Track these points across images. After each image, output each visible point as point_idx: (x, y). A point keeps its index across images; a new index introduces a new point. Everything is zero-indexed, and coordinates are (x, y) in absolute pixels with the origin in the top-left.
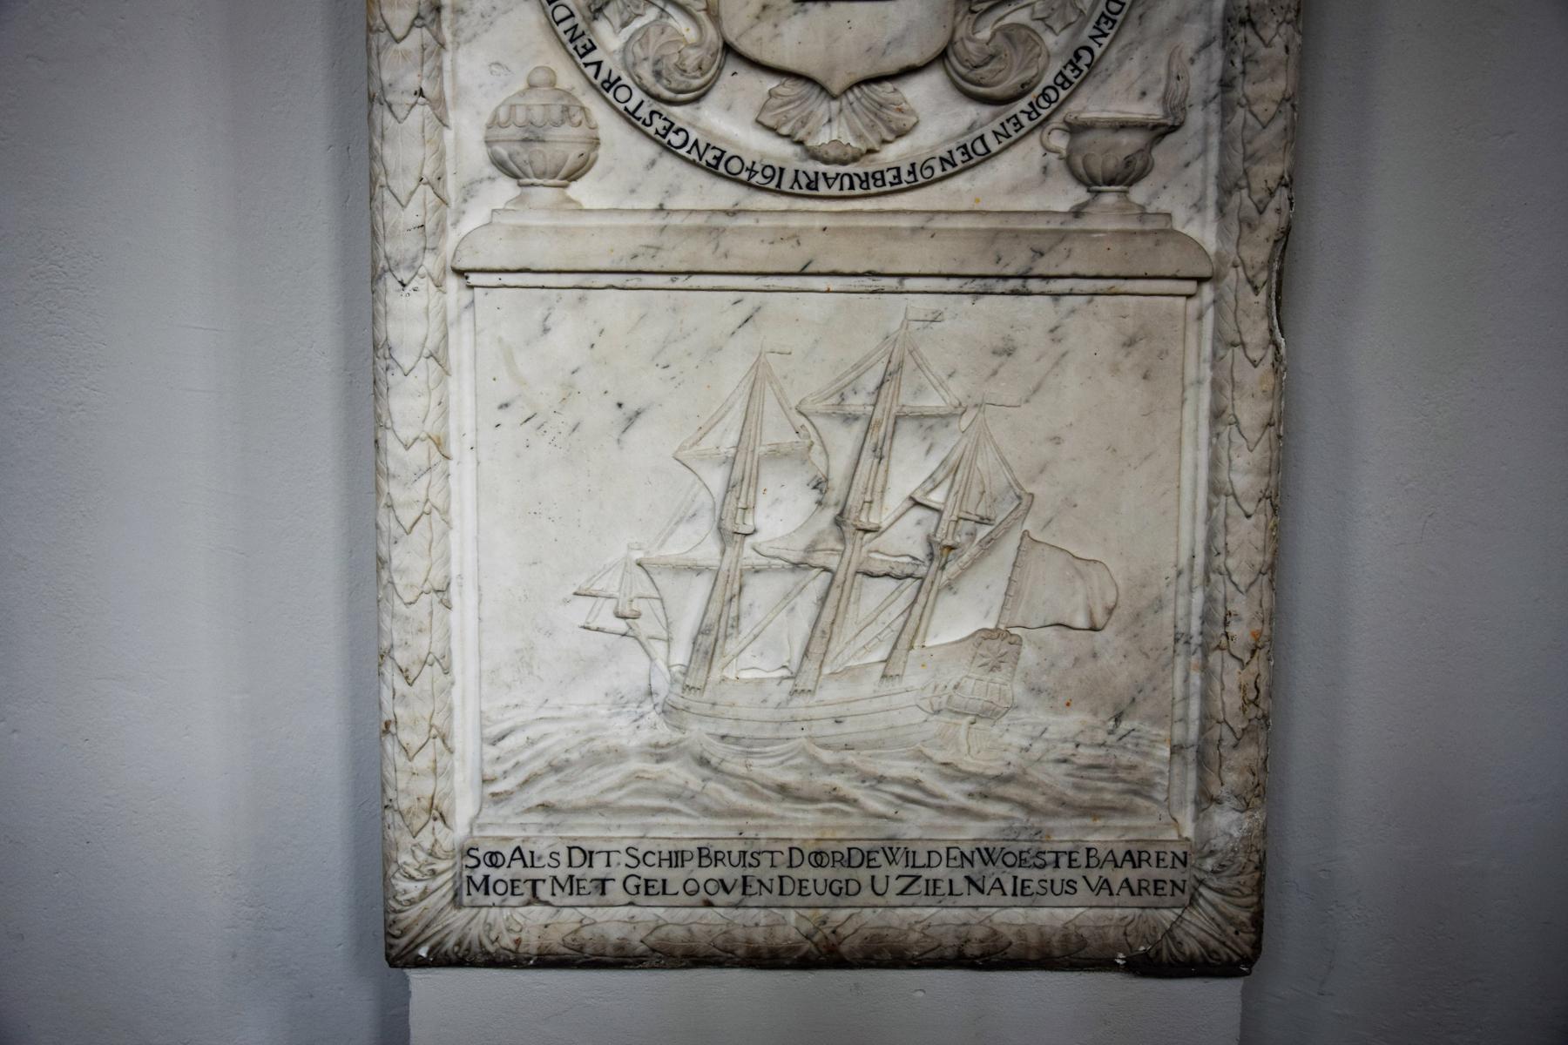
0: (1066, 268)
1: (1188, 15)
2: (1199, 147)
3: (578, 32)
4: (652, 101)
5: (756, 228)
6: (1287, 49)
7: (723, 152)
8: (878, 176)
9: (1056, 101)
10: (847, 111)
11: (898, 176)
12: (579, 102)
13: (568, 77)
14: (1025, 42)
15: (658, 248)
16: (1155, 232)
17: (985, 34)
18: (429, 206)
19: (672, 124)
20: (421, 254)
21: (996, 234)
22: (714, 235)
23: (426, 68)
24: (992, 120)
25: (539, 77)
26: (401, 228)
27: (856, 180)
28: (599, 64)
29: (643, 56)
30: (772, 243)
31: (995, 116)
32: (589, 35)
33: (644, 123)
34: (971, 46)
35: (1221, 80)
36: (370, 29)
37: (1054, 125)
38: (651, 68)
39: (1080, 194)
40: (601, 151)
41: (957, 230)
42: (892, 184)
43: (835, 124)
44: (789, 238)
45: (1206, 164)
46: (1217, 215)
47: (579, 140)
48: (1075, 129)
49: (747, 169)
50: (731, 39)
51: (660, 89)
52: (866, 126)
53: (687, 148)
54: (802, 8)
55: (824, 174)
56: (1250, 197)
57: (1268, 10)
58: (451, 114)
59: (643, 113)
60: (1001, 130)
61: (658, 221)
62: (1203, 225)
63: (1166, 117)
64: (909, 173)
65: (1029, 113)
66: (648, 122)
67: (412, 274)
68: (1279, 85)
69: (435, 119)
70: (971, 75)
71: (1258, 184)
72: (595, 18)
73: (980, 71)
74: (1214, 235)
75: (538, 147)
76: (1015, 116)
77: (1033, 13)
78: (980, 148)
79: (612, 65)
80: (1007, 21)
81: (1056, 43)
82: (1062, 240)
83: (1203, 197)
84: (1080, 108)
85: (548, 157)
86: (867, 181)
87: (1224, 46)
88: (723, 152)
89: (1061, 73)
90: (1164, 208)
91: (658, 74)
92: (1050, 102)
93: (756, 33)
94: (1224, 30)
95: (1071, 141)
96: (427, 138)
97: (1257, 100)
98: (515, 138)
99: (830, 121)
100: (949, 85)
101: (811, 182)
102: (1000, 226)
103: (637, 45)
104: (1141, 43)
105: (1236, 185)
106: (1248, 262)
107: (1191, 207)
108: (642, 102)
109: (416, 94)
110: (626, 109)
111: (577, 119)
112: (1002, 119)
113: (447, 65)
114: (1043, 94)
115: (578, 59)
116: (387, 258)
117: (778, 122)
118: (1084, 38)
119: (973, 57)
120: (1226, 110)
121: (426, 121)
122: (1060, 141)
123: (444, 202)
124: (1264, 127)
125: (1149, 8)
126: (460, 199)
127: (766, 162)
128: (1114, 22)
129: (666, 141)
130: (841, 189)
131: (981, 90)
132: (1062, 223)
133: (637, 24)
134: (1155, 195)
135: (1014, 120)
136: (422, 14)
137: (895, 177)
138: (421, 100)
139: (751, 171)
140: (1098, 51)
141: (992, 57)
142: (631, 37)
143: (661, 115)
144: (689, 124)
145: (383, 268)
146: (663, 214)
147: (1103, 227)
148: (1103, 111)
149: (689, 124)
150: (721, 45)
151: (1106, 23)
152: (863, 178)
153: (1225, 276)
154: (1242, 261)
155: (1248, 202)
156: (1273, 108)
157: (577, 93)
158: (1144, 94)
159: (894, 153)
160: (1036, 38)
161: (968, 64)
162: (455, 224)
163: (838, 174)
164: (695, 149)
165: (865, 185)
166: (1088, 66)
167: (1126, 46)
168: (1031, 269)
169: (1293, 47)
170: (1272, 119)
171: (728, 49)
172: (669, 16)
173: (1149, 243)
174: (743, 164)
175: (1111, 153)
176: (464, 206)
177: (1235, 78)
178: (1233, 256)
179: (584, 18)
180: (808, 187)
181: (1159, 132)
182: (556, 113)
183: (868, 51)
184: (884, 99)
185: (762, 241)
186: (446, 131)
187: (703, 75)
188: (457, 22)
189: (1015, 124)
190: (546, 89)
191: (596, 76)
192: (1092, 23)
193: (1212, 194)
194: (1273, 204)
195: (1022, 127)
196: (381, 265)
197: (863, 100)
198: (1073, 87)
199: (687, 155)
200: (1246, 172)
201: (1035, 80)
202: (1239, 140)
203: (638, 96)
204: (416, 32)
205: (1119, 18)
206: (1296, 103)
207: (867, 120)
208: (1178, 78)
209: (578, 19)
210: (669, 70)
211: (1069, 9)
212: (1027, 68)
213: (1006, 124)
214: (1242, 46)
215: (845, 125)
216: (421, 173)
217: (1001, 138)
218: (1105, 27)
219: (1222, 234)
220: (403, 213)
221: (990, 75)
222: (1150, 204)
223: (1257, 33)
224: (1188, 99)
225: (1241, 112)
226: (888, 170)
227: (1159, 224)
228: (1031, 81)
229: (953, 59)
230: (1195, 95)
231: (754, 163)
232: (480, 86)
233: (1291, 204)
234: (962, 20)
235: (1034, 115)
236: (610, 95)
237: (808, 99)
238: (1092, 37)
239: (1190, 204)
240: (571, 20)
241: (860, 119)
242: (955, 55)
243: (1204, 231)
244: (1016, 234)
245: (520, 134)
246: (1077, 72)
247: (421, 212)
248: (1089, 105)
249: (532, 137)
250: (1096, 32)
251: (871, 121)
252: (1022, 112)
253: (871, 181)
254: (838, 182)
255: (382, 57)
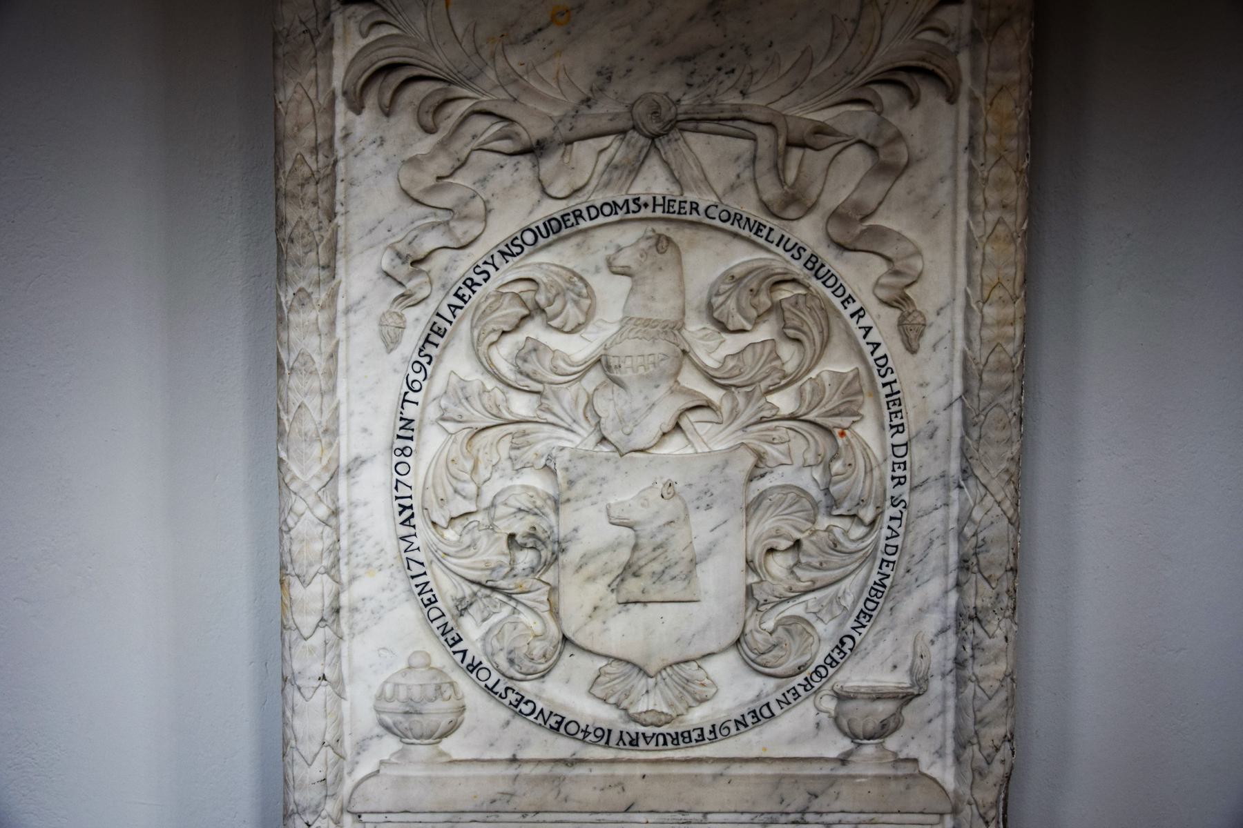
0: (837, 806)
1: (928, 607)
2: (939, 708)
3: (448, 628)
4: (506, 679)
5: (588, 776)
6: (1006, 639)
7: (563, 718)
8: (686, 735)
9: (826, 676)
10: (661, 685)
11: (702, 734)
12: (450, 678)
13: (440, 657)
14: (801, 634)
15: (512, 795)
16: (906, 777)
17: (770, 624)
18: (330, 763)
19: (523, 697)
20: (323, 801)
21: (780, 778)
22: (556, 783)
23: (328, 658)
24: (775, 692)
25: (417, 661)
26: (307, 782)
27: (669, 738)
28: (465, 652)
29: (499, 647)
30: (603, 790)
31: (778, 687)
32: (456, 630)
33: (500, 696)
34: (757, 636)
35: (956, 659)
36: (284, 627)
37: (824, 692)
38: (506, 656)
39: (845, 744)
40: (466, 714)
41: (748, 777)
42: (697, 741)
43: (652, 695)
44: (616, 786)
45: (945, 720)
46: (954, 763)
47: (449, 711)
48: (841, 697)
49: (582, 731)
50: (569, 635)
51: (513, 672)
52: (676, 697)
53: (535, 715)
54: (625, 608)
55: (643, 734)
56: (980, 750)
57: (991, 611)
58: (348, 689)
59: (500, 688)
60: (783, 699)
61: (512, 771)
62: (944, 768)
63: (912, 686)
64: (711, 732)
65: (805, 686)
66: (504, 695)
67: (315, 817)
68: (1002, 667)
69: (335, 695)
70: (759, 660)
71: (986, 743)
72: (461, 615)
73: (764, 656)
74: (953, 776)
75: (416, 717)
76: (794, 688)
77: (807, 608)
78: (766, 712)
79: (475, 651)
80: (787, 613)
81: (825, 630)
82: (832, 785)
83: (943, 746)
84: (845, 679)
85: (425, 725)
86: (677, 738)
87: (957, 633)
88: (563, 718)
89: (829, 655)
90: (912, 754)
91: (511, 661)
92: (821, 677)
93: (588, 629)
94: (956, 620)
95: (837, 706)
96: (328, 712)
97: (984, 678)
98: (398, 711)
99: (647, 692)
100: (741, 662)
101: (633, 740)
102: (782, 772)
103: (495, 640)
104: (892, 629)
105: (969, 742)
106: (980, 802)
107: (934, 753)
108: (499, 681)
109: (319, 679)
110: (486, 686)
111: (447, 695)
112: (784, 690)
113: (345, 653)
114: (816, 671)
115: (448, 648)
116: (297, 805)
117: (606, 695)
118: (847, 629)
119: (760, 646)
120: (960, 683)
121: (328, 698)
122: (829, 704)
123: (342, 757)
124: (990, 699)
125: (898, 602)
126: (354, 753)
127: (598, 725)
128: (871, 616)
129: (518, 710)
130: (657, 745)
131: (767, 670)
132: (832, 770)
133: (494, 619)
134: (905, 744)
135: (793, 691)
136: (325, 618)
137: (699, 736)
138: (324, 682)
139: (586, 732)
140: (858, 639)
141: (775, 646)
142: (490, 630)
143: (514, 690)
144: (536, 696)
145: (292, 810)
146: (515, 765)
147: (864, 773)
148: (863, 680)
149: (536, 696)
150: (561, 637)
151: (865, 617)
152: (674, 736)
153: (962, 811)
154: (975, 801)
155: (978, 755)
156: (997, 684)
157: (447, 670)
158: (895, 667)
159: (698, 716)
160: (809, 629)
161: (756, 651)
162: (350, 773)
163: (654, 734)
164: (541, 715)
165: (675, 742)
166: (851, 650)
167: (880, 631)
168: (808, 808)
169: (1011, 636)
170: (997, 692)
171: (565, 639)
172: (519, 612)
173: (901, 786)
174: (579, 727)
175: (870, 718)
176: (357, 759)
177: (966, 660)
178: (968, 797)
179: (453, 616)
180: (631, 743)
181: (905, 698)
182: (431, 691)
183: (677, 641)
184: (689, 675)
185: (595, 788)
186: (343, 702)
187: (546, 662)
188: (353, 617)
189: (794, 694)
190: (423, 669)
191: (462, 661)
192: (854, 617)
193: (950, 745)
194: (999, 756)
195: (799, 696)
196: (291, 808)
197: (674, 677)
198: (839, 665)
199: (534, 720)
200: (976, 733)
201: (809, 663)
202: (971, 707)
203: (495, 676)
204: (320, 631)
205: (874, 613)
206: (1015, 677)
207: (677, 692)
208: (922, 656)
209: (448, 618)
210: (520, 658)
211: (835, 606)
212: (802, 654)
213: (787, 694)
214: (971, 636)
215: (659, 695)
216: (324, 739)
217: (783, 705)
218: (863, 621)
219: (959, 776)
220: (309, 770)
221: (773, 660)
222: (901, 751)
223: (982, 627)
224: (930, 671)
225: (971, 686)
226: (694, 730)
227: (908, 769)
228: (806, 664)
229: (745, 646)
230: (935, 668)
231: (587, 726)
232: (371, 666)
233: (1013, 754)
234: (751, 616)
235: (809, 687)
236: (473, 675)
237: (630, 676)
238: (854, 628)
239: (933, 751)
240: (443, 618)
241: (671, 691)
242: (746, 643)
243: (945, 774)
244: (796, 779)
245: (403, 708)
246: (842, 655)
247: (323, 769)
248: (852, 677)
249: (412, 710)
250: (857, 624)
251: (681, 692)
252: (799, 685)
253: (681, 739)
254: (654, 739)
255: (293, 650)
